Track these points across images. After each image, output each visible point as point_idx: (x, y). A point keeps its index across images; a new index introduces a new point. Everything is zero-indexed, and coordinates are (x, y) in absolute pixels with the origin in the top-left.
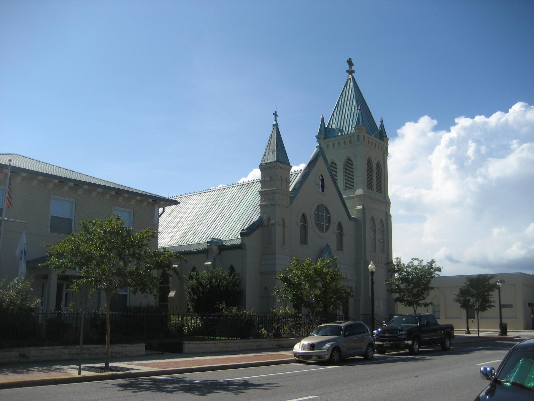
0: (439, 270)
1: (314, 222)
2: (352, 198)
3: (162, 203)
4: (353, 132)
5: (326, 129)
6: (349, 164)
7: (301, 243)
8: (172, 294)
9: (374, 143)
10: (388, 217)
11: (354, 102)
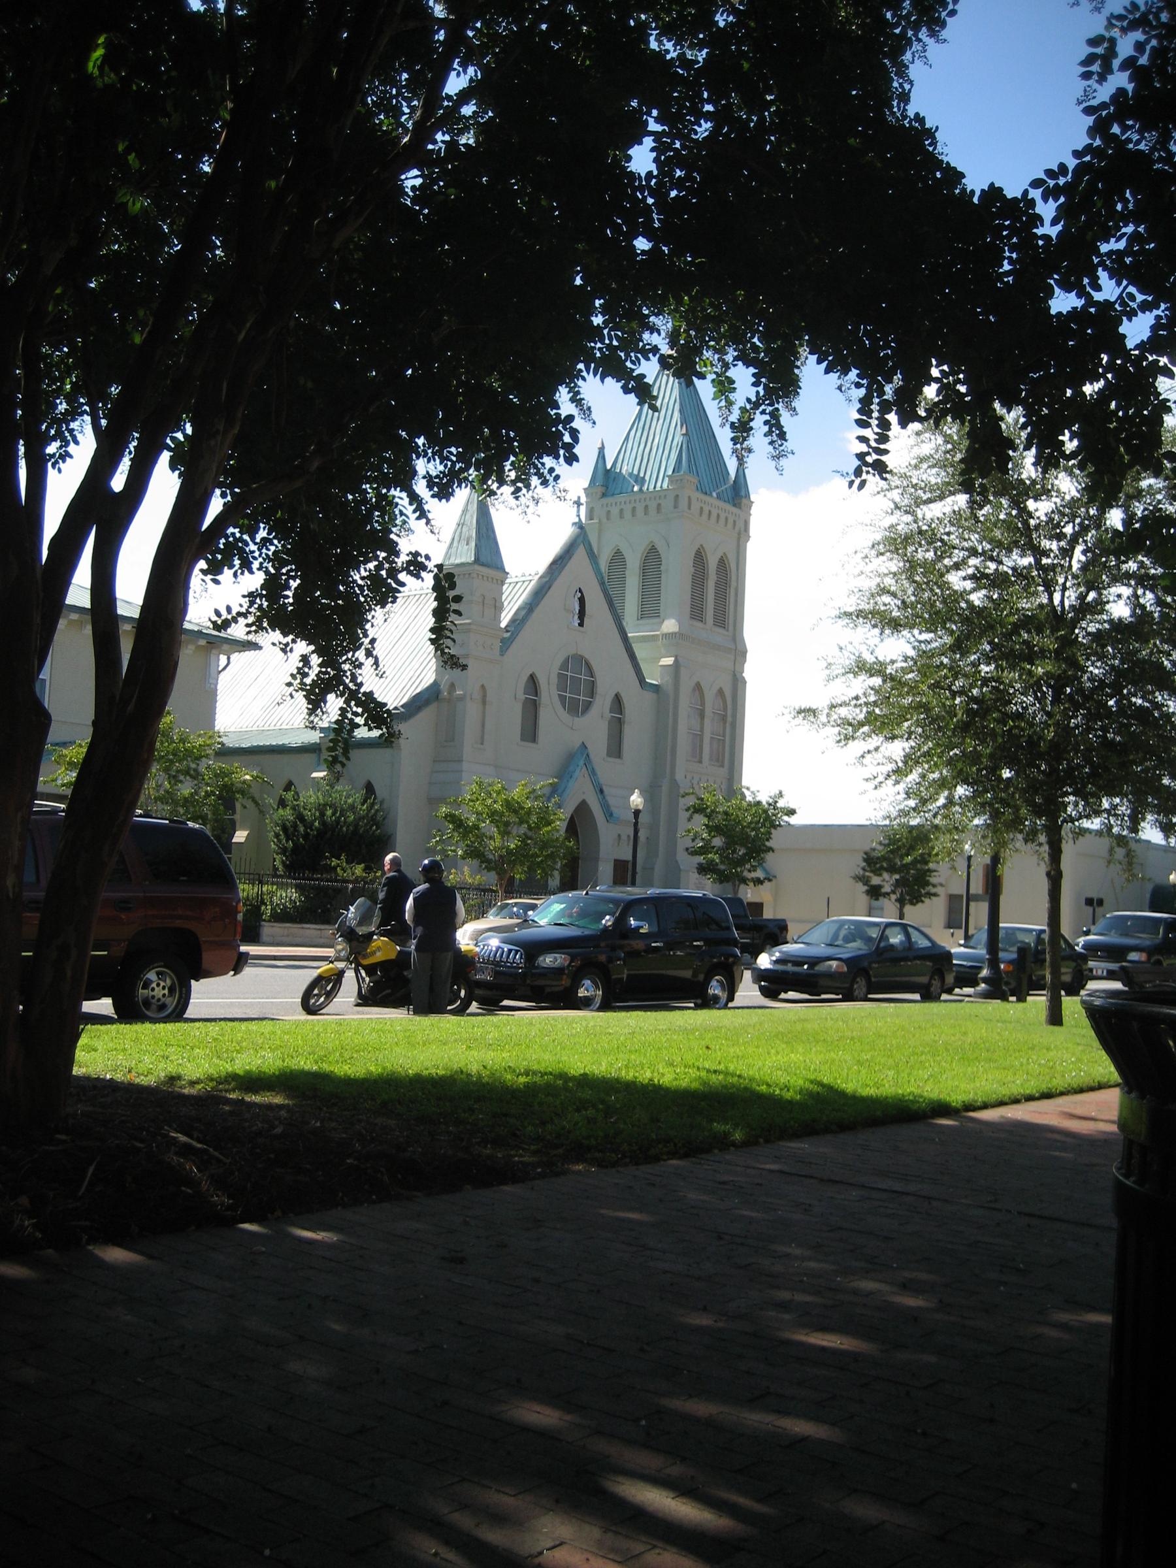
0: (792, 812)
1: (555, 693)
2: (654, 638)
3: (226, 647)
4: (665, 486)
5: (607, 472)
6: (652, 559)
7: (522, 739)
8: (240, 836)
9: (714, 513)
10: (738, 683)
11: (677, 414)
